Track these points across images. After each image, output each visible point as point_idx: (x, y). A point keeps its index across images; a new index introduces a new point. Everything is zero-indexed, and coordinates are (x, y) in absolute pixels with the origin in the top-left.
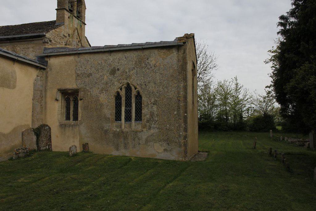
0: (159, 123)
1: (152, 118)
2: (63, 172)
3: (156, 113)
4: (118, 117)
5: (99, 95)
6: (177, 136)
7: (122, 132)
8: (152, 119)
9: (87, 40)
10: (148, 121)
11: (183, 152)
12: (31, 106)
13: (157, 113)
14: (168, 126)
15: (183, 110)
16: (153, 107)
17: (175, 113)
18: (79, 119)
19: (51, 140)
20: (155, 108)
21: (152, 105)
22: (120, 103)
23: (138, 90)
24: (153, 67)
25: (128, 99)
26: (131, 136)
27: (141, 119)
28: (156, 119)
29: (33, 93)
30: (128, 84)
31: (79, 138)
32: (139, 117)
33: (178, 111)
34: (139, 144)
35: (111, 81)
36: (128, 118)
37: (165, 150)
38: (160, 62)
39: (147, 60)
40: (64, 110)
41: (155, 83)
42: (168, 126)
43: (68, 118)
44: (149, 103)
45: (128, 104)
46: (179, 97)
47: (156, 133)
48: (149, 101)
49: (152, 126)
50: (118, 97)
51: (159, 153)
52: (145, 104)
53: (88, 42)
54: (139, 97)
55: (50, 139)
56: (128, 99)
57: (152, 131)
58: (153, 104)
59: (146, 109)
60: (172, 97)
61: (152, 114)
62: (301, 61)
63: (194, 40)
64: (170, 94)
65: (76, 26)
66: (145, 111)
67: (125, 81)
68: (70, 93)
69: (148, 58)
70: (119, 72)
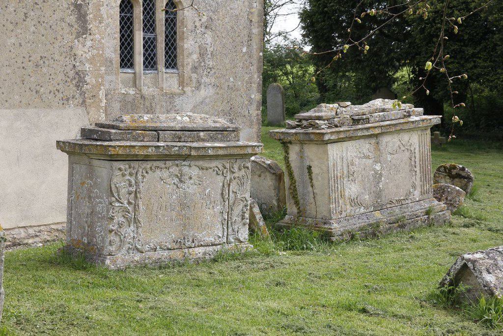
0: (215, 73)
1: (204, 61)
2: (20, 36)
3: (210, 50)
4: (127, 61)
7: (143, 97)
8: (203, 64)
11: (255, 136)
13: (212, 49)
14: (232, 79)
16: (206, 35)
20: (209, 38)
21: (203, 29)
22: (128, 19)
26: (162, 106)
27: (175, 64)
28: (211, 63)
32: (172, 61)
33: (249, 46)
36: (150, 62)
42: (232, 79)
44: (198, 24)
46: (252, 13)
48: (197, 19)
49: (203, 81)
52: (190, 25)
57: (203, 93)
59: (191, 38)
60: (240, 14)
62: (76, 29)
64: (236, 6)
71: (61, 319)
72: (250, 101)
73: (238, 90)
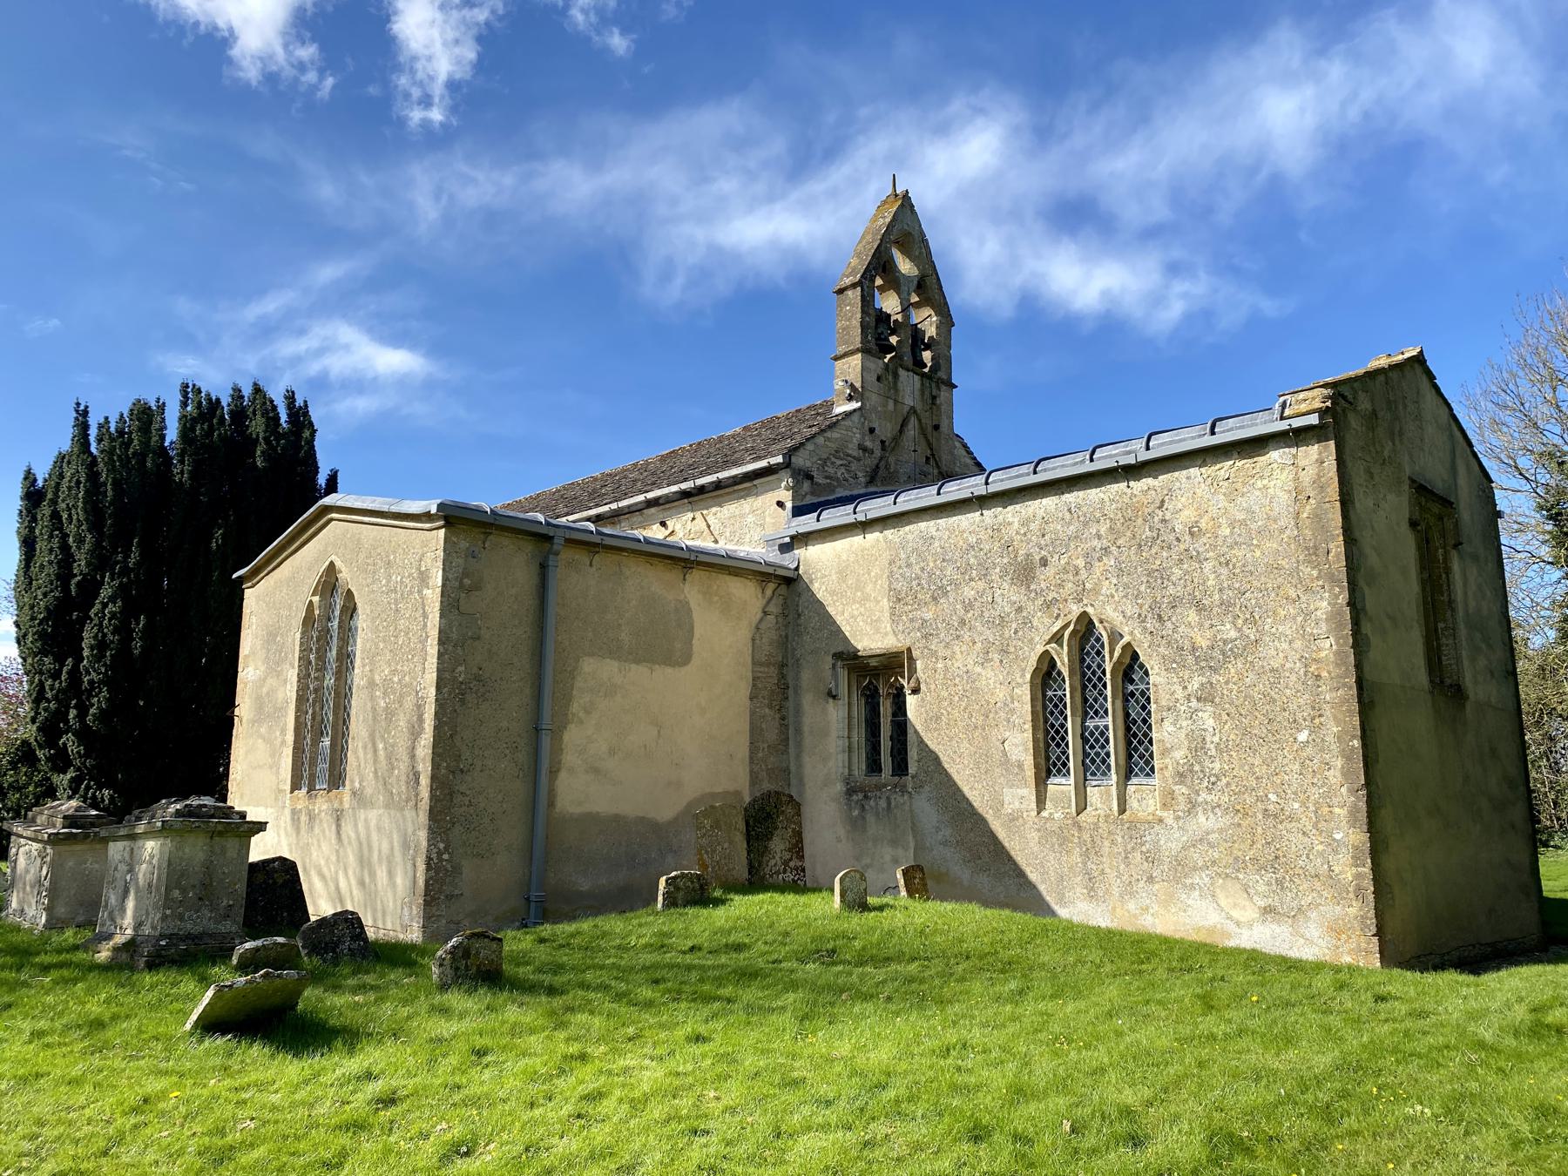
0: (1228, 784)
3: (1212, 740)
5: (978, 669)
6: (1320, 848)
9: (965, 446)
10: (1181, 777)
12: (744, 725)
14: (1273, 797)
15: (1338, 722)
17: (1303, 736)
18: (912, 770)
19: (802, 849)
20: (1207, 719)
21: (1194, 703)
23: (1129, 644)
24: (1187, 537)
25: (1087, 679)
29: (750, 675)
30: (1084, 615)
31: (912, 845)
34: (1151, 879)
35: (1019, 610)
37: (1268, 911)
38: (1213, 511)
39: (1160, 508)
40: (859, 736)
41: (1200, 607)
42: (1273, 797)
43: (874, 766)
45: (1087, 708)
47: (1221, 831)
50: (1046, 673)
51: (1238, 924)
53: (970, 453)
54: (1131, 666)
55: (796, 845)
56: (1087, 679)
57: (1203, 821)
58: (1199, 700)
59: (1167, 726)
61: (1198, 746)
63: (1431, 377)
65: (909, 402)
66: (1166, 732)
67: (1075, 610)
68: (876, 668)
69: (1163, 501)
70: (1050, 571)
71: (450, 897)
72: (1334, 846)
73: (1291, 819)
